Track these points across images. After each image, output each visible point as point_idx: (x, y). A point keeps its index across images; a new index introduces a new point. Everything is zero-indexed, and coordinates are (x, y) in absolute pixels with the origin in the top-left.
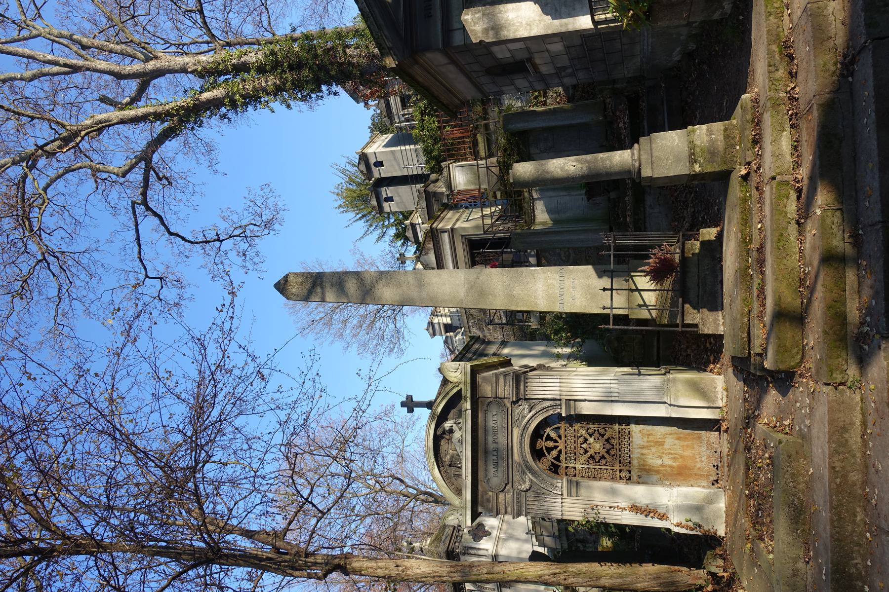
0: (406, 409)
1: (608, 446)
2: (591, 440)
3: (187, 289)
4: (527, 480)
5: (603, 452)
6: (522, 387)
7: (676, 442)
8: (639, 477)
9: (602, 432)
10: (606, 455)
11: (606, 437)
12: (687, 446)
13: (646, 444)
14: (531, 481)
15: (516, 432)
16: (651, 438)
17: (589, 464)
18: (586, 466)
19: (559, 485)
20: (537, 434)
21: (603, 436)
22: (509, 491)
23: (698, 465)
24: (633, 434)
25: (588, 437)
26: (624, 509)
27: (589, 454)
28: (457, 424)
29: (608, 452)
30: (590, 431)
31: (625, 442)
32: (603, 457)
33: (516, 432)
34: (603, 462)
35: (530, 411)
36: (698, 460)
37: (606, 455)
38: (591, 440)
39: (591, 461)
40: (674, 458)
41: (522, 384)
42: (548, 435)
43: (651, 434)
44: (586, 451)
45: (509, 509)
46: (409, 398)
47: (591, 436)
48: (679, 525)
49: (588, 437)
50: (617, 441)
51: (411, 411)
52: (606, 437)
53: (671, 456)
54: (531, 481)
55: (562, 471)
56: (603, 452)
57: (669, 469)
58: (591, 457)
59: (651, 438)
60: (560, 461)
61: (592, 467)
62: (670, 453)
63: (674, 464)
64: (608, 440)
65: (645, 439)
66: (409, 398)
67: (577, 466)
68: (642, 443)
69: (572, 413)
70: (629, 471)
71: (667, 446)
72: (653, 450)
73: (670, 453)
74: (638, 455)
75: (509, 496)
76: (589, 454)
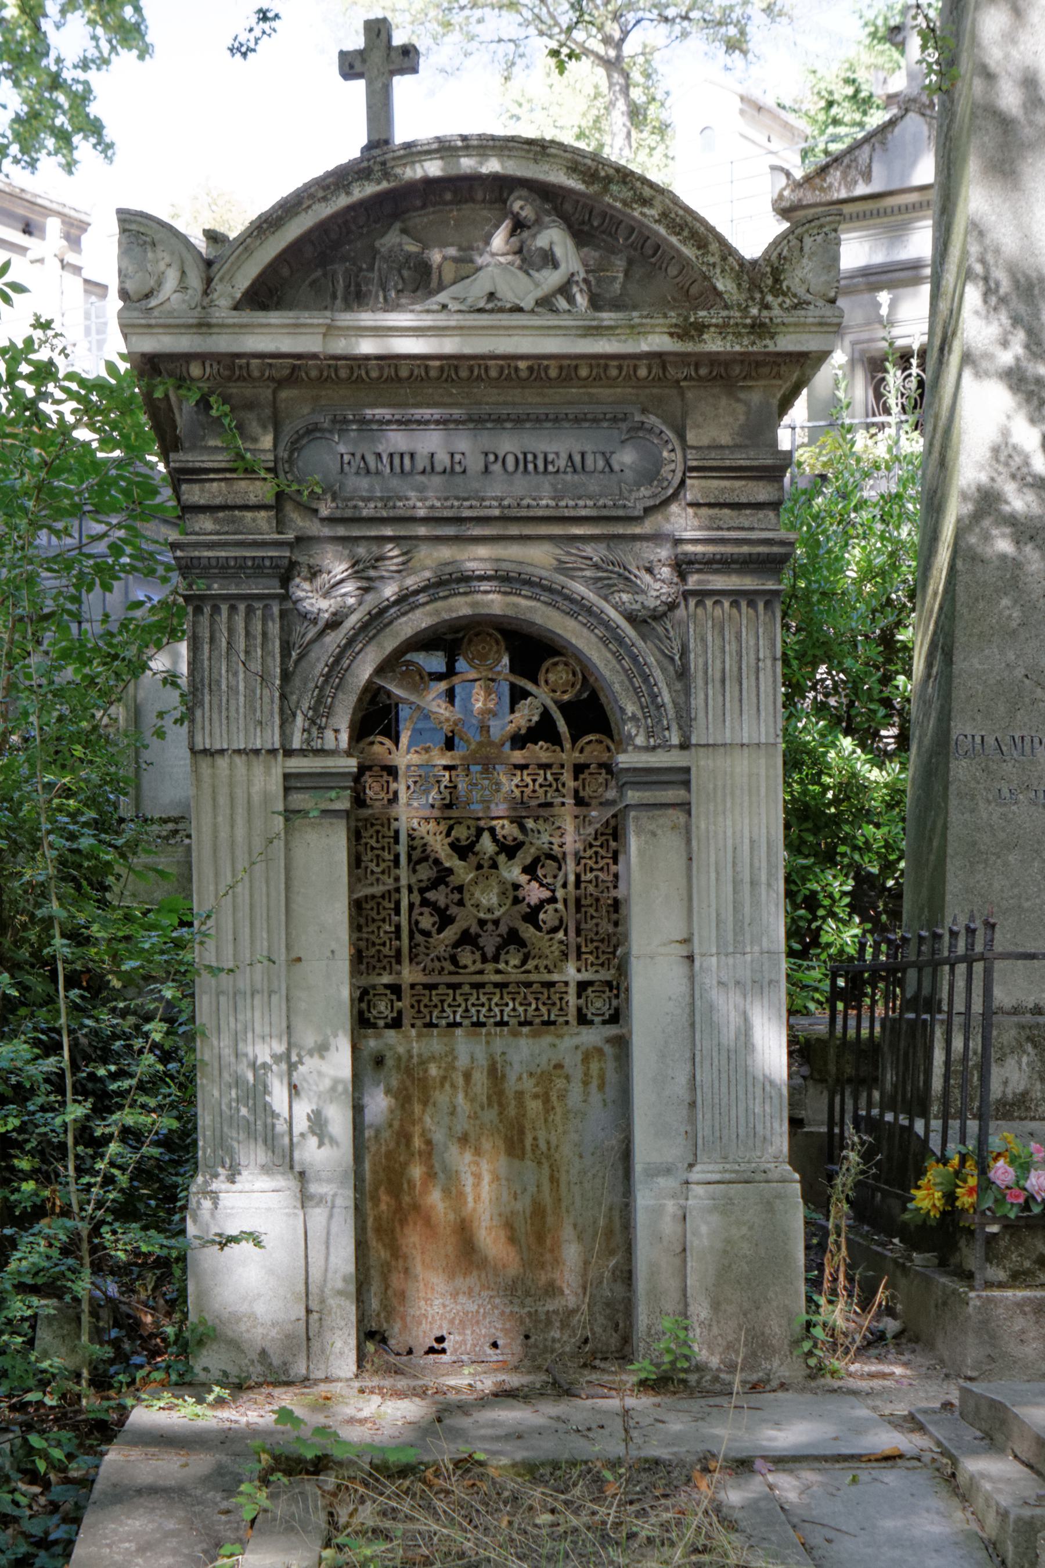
0: (398, 39)
1: (489, 943)
3: (89, 55)
5: (464, 920)
8: (379, 1061)
10: (451, 933)
11: (528, 932)
13: (511, 1085)
18: (402, 849)
24: (547, 1040)
26: (356, 1510)
28: (564, 290)
29: (466, 939)
34: (427, 922)
37: (451, 933)
41: (748, 583)
42: (555, 739)
46: (407, 59)
50: (515, 976)
51: (350, 66)
52: (528, 932)
56: (464, 920)
59: (534, 1106)
64: (513, 938)
66: (407, 59)
70: (396, 1024)
74: (463, 1061)
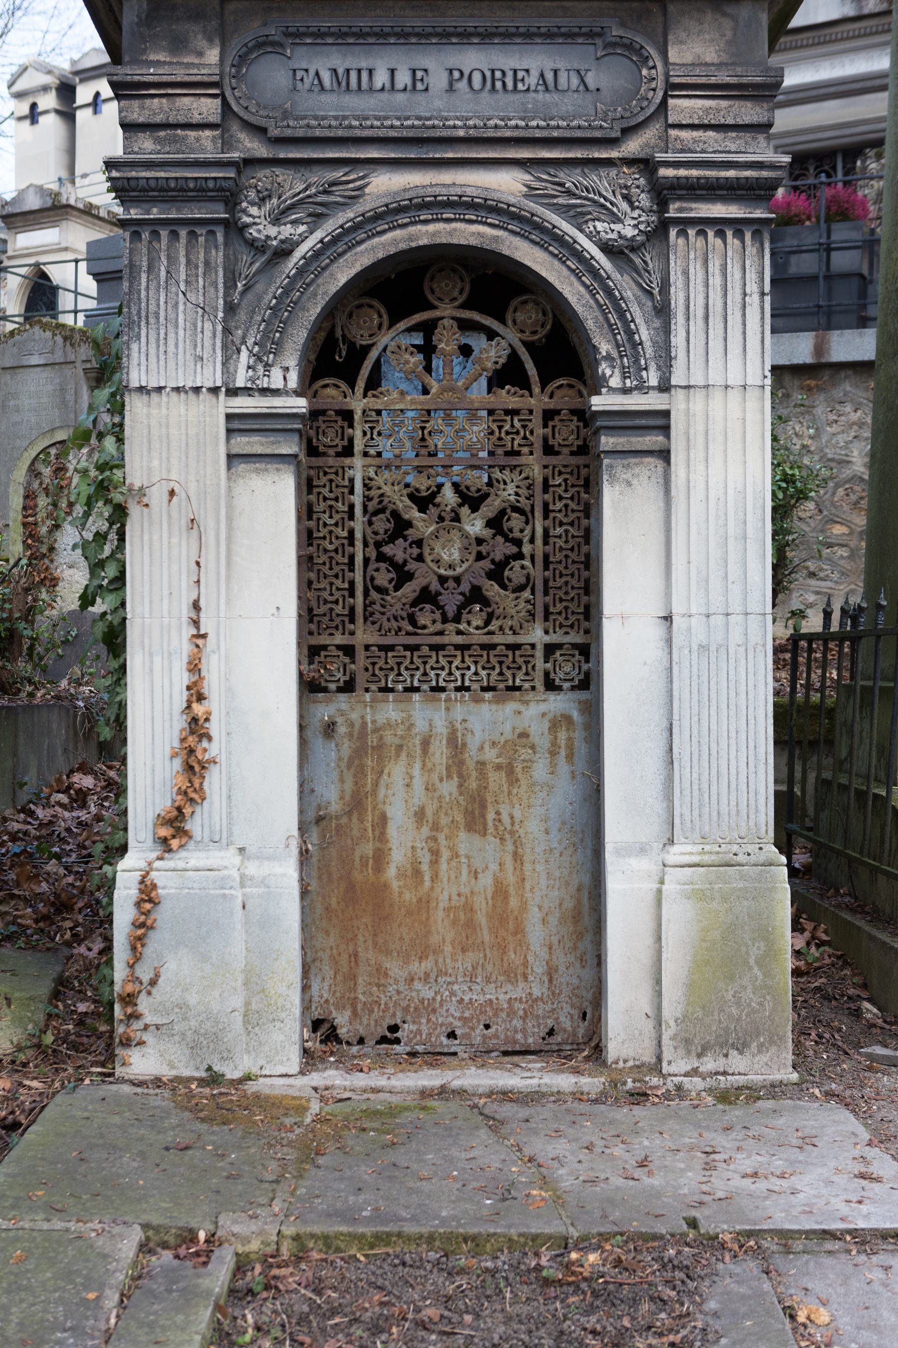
1: (451, 601)
2: (475, 525)
4: (287, 231)
6: (719, 210)
7: (486, 881)
8: (329, 729)
9: (515, 573)
10: (410, 590)
11: (492, 589)
12: (470, 925)
13: (471, 755)
14: (284, 251)
15: (506, 184)
16: (496, 779)
17: (371, 514)
18: (357, 499)
19: (276, 380)
20: (496, 285)
21: (497, 574)
22: (227, 144)
23: (394, 967)
24: (511, 707)
25: (489, 509)
27: (414, 514)
30: (515, 522)
31: (474, 672)
32: (403, 576)
33: (506, 184)
34: (384, 578)
35: (607, 248)
36: (417, 967)
37: (410, 590)
38: (475, 525)
39: (382, 524)
40: (417, 873)
43: (513, 780)
44: (423, 502)
45: (147, 145)
47: (495, 523)
48: (148, 895)
49: (489, 509)
50: (479, 637)
52: (492, 589)
53: (425, 858)
54: (284, 251)
55: (333, 394)
56: (424, 576)
57: (368, 849)
58: (401, 526)
59: (496, 779)
60: (514, 356)
61: (359, 525)
62: (435, 854)
63: (391, 872)
64: (476, 596)
65: (490, 755)
67: (358, 461)
68: (473, 743)
69: (607, 442)
70: (348, 687)
71: (465, 842)
72: (448, 788)
73: (435, 854)
74: (421, 725)
75: (206, 144)
76: (414, 514)
